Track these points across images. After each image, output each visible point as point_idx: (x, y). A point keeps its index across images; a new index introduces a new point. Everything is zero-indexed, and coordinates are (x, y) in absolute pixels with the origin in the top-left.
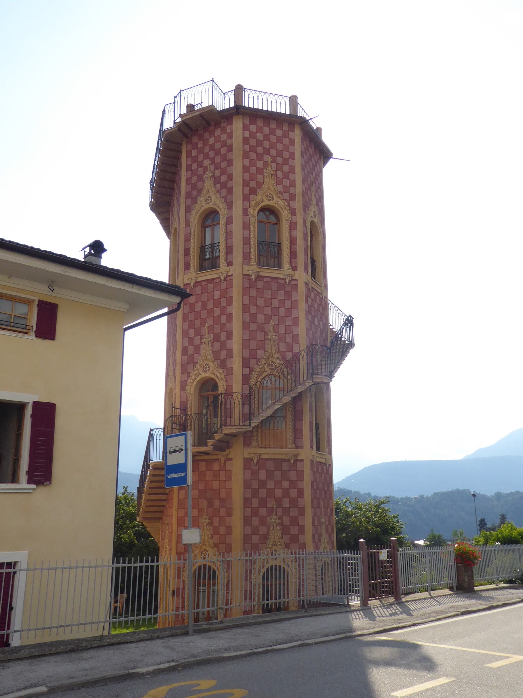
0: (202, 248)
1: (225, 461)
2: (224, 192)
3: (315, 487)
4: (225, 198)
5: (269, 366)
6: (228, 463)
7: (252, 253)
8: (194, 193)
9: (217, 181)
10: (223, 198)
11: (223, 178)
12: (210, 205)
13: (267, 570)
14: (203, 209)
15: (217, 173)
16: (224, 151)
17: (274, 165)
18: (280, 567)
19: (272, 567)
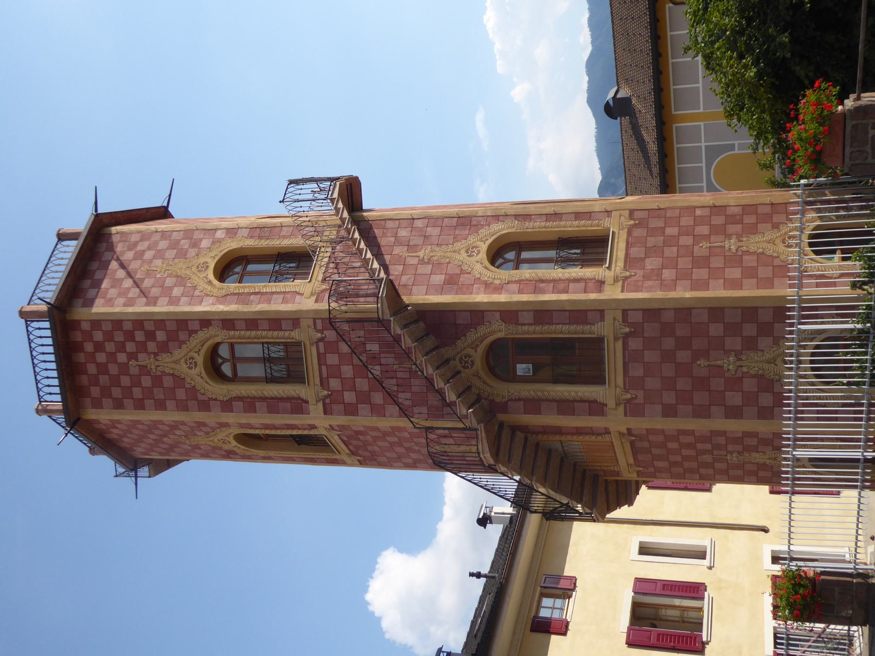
0: (270, 380)
1: (632, 435)
2: (183, 336)
3: (682, 439)
4: (192, 332)
5: (468, 367)
6: (634, 432)
7: (281, 334)
8: (181, 394)
9: (164, 348)
10: (190, 336)
11: (161, 336)
12: (200, 359)
13: (817, 253)
14: (204, 374)
15: (151, 346)
16: (116, 392)
17: (141, 356)
18: (811, 236)
19: (811, 245)
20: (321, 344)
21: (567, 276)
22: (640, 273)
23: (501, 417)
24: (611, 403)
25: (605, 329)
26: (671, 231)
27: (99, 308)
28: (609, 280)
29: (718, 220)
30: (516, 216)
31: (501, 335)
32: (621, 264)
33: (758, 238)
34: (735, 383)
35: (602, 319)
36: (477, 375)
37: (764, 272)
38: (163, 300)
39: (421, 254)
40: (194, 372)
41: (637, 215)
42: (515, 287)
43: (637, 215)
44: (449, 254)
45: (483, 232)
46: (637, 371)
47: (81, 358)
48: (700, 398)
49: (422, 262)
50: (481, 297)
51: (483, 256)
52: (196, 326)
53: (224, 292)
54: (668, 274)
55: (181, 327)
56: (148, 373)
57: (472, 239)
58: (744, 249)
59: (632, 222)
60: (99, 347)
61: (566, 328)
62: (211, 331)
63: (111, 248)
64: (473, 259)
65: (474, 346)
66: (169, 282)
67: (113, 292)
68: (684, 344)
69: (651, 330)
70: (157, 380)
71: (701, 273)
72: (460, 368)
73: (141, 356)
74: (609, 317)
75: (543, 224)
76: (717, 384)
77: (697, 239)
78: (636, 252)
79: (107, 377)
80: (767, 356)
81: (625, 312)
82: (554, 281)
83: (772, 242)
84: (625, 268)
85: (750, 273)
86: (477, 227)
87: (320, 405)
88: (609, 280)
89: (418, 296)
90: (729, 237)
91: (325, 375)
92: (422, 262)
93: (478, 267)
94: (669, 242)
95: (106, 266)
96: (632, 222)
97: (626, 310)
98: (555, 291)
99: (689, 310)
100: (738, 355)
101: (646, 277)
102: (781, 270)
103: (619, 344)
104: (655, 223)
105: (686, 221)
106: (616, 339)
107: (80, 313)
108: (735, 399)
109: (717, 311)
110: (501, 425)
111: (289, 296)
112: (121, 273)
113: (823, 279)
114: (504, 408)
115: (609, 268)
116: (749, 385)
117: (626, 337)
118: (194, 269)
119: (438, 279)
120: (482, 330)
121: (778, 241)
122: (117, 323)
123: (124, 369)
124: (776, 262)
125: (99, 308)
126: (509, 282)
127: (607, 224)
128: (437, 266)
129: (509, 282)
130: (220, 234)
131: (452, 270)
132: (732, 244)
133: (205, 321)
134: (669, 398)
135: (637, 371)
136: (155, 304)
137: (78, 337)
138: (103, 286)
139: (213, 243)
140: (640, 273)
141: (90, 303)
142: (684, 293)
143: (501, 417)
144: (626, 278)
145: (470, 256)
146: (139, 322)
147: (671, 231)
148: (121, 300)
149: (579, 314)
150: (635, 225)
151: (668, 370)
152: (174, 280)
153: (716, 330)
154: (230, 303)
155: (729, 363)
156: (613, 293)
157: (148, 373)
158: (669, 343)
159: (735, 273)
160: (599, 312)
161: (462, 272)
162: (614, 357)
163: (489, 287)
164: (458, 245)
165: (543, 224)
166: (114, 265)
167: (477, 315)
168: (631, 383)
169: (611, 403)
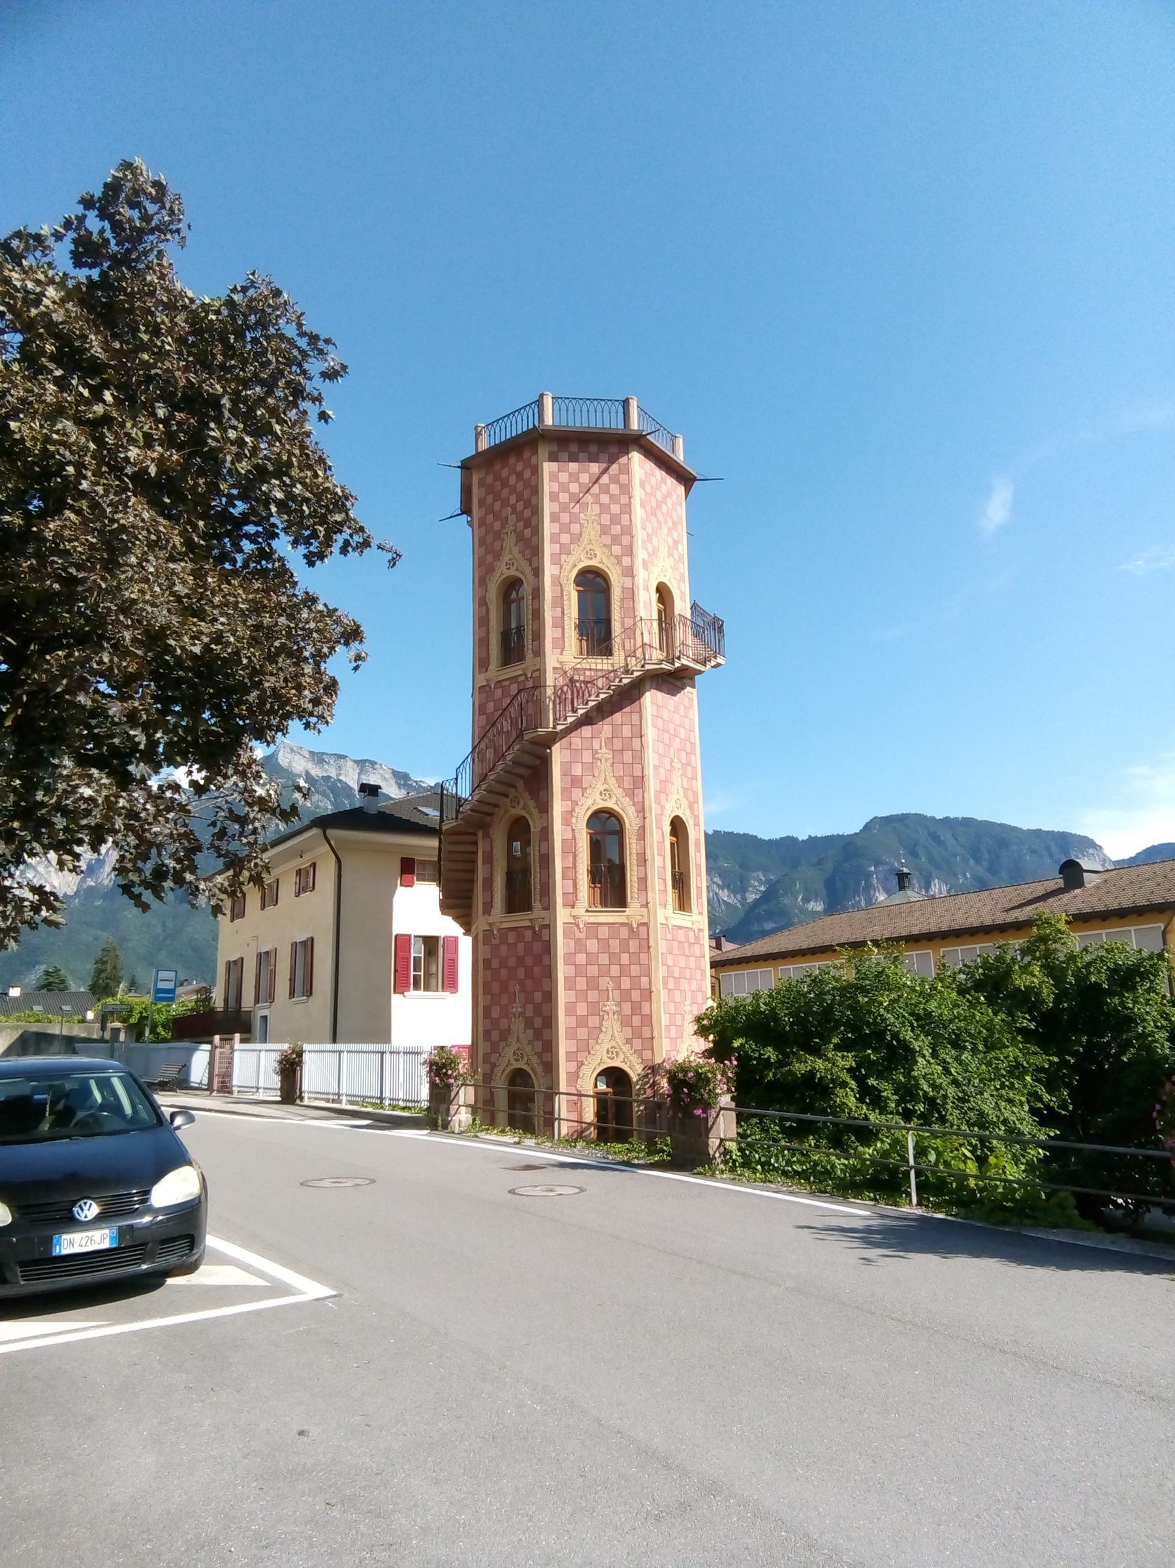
4: (530, 561)
17: (514, 516)
20: (522, 678)
21: (580, 877)
22: (583, 936)
23: (480, 834)
24: (491, 919)
25: (537, 912)
26: (625, 959)
27: (548, 468)
28: (575, 912)
29: (636, 995)
30: (643, 827)
31: (532, 829)
32: (592, 920)
33: (617, 1026)
34: (506, 1014)
35: (544, 909)
36: (506, 811)
37: (582, 1033)
38: (556, 528)
39: (604, 750)
40: (504, 567)
41: (545, 932)
42: (569, 836)
43: (643, 930)
44: (603, 775)
45: (627, 801)
46: (511, 938)
47: (512, 461)
48: (496, 986)
49: (595, 752)
50: (558, 808)
51: (601, 804)
52: (534, 565)
53: (564, 582)
54: (581, 958)
55: (533, 550)
56: (503, 527)
57: (619, 792)
58: (606, 1017)
59: (635, 926)
60: (519, 475)
61: (538, 880)
62: (531, 579)
63: (612, 460)
64: (598, 797)
65: (524, 807)
66: (575, 528)
67: (564, 477)
68: (529, 973)
69: (537, 947)
70: (498, 536)
71: (581, 983)
72: (511, 796)
73: (514, 516)
74: (544, 913)
75: (634, 851)
76: (504, 999)
77: (617, 981)
78: (604, 932)
79: (499, 488)
80: (522, 1036)
81: (646, 925)
82: (575, 866)
83: (613, 1038)
84: (588, 924)
85: (582, 1022)
86: (630, 793)
87: (485, 683)
88: (575, 912)
89: (558, 755)
90: (619, 1004)
91: (505, 684)
92: (595, 752)
93: (589, 802)
94: (614, 958)
95: (593, 459)
96: (635, 926)
97: (550, 927)
98: (565, 869)
99: (550, 976)
100: (522, 1014)
101: (578, 942)
102: (585, 1047)
103: (527, 923)
104: (633, 945)
105: (635, 970)
106: (531, 920)
107: (543, 450)
108: (495, 1013)
109: (550, 997)
110: (475, 834)
111: (560, 642)
112: (585, 478)
113: (574, 1077)
114: (486, 835)
115: (587, 911)
116: (504, 1023)
117: (532, 928)
118: (590, 547)
119: (577, 770)
120: (535, 812)
121: (613, 1043)
122: (536, 490)
123: (505, 503)
124: (592, 1042)
125: (548, 468)
126: (573, 830)
127: (632, 905)
128: (590, 768)
129: (573, 830)
130: (626, 561)
131: (586, 781)
132: (611, 1006)
133: (538, 572)
134: (495, 964)
135: (511, 938)
136: (552, 521)
137: (526, 455)
138: (571, 464)
139: (616, 557)
140: (583, 936)
141: (553, 458)
142: (562, 971)
143: (480, 834)
144: (578, 926)
145: (601, 794)
146: (537, 511)
147: (625, 959)
148: (555, 487)
149: (547, 890)
150: (534, 932)
151: (512, 962)
152: (578, 532)
153: (538, 997)
154: (553, 591)
155: (517, 1009)
156: (562, 915)
157: (503, 527)
158: (529, 961)
159: (582, 1009)
160: (549, 906)
161: (584, 790)
162: (520, 920)
163: (568, 817)
164: (613, 782)
165: (634, 851)
166: (595, 468)
167: (545, 807)
168: (504, 932)
169: (491, 919)
